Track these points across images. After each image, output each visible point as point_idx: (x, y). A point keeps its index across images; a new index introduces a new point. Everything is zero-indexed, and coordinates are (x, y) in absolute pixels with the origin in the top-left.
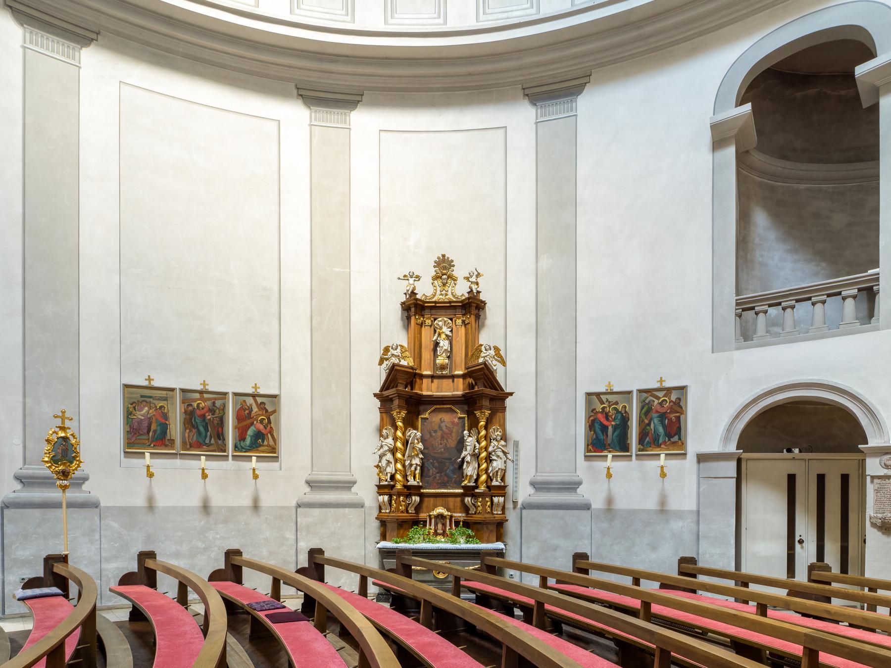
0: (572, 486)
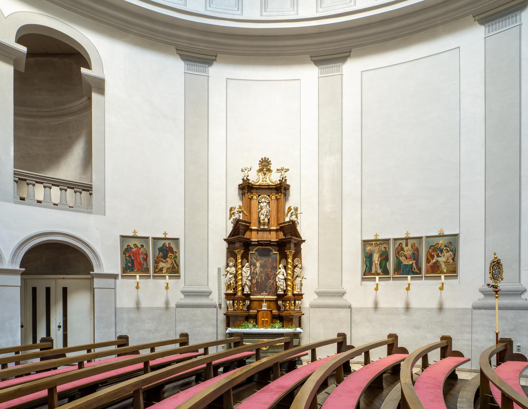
0: (342, 294)
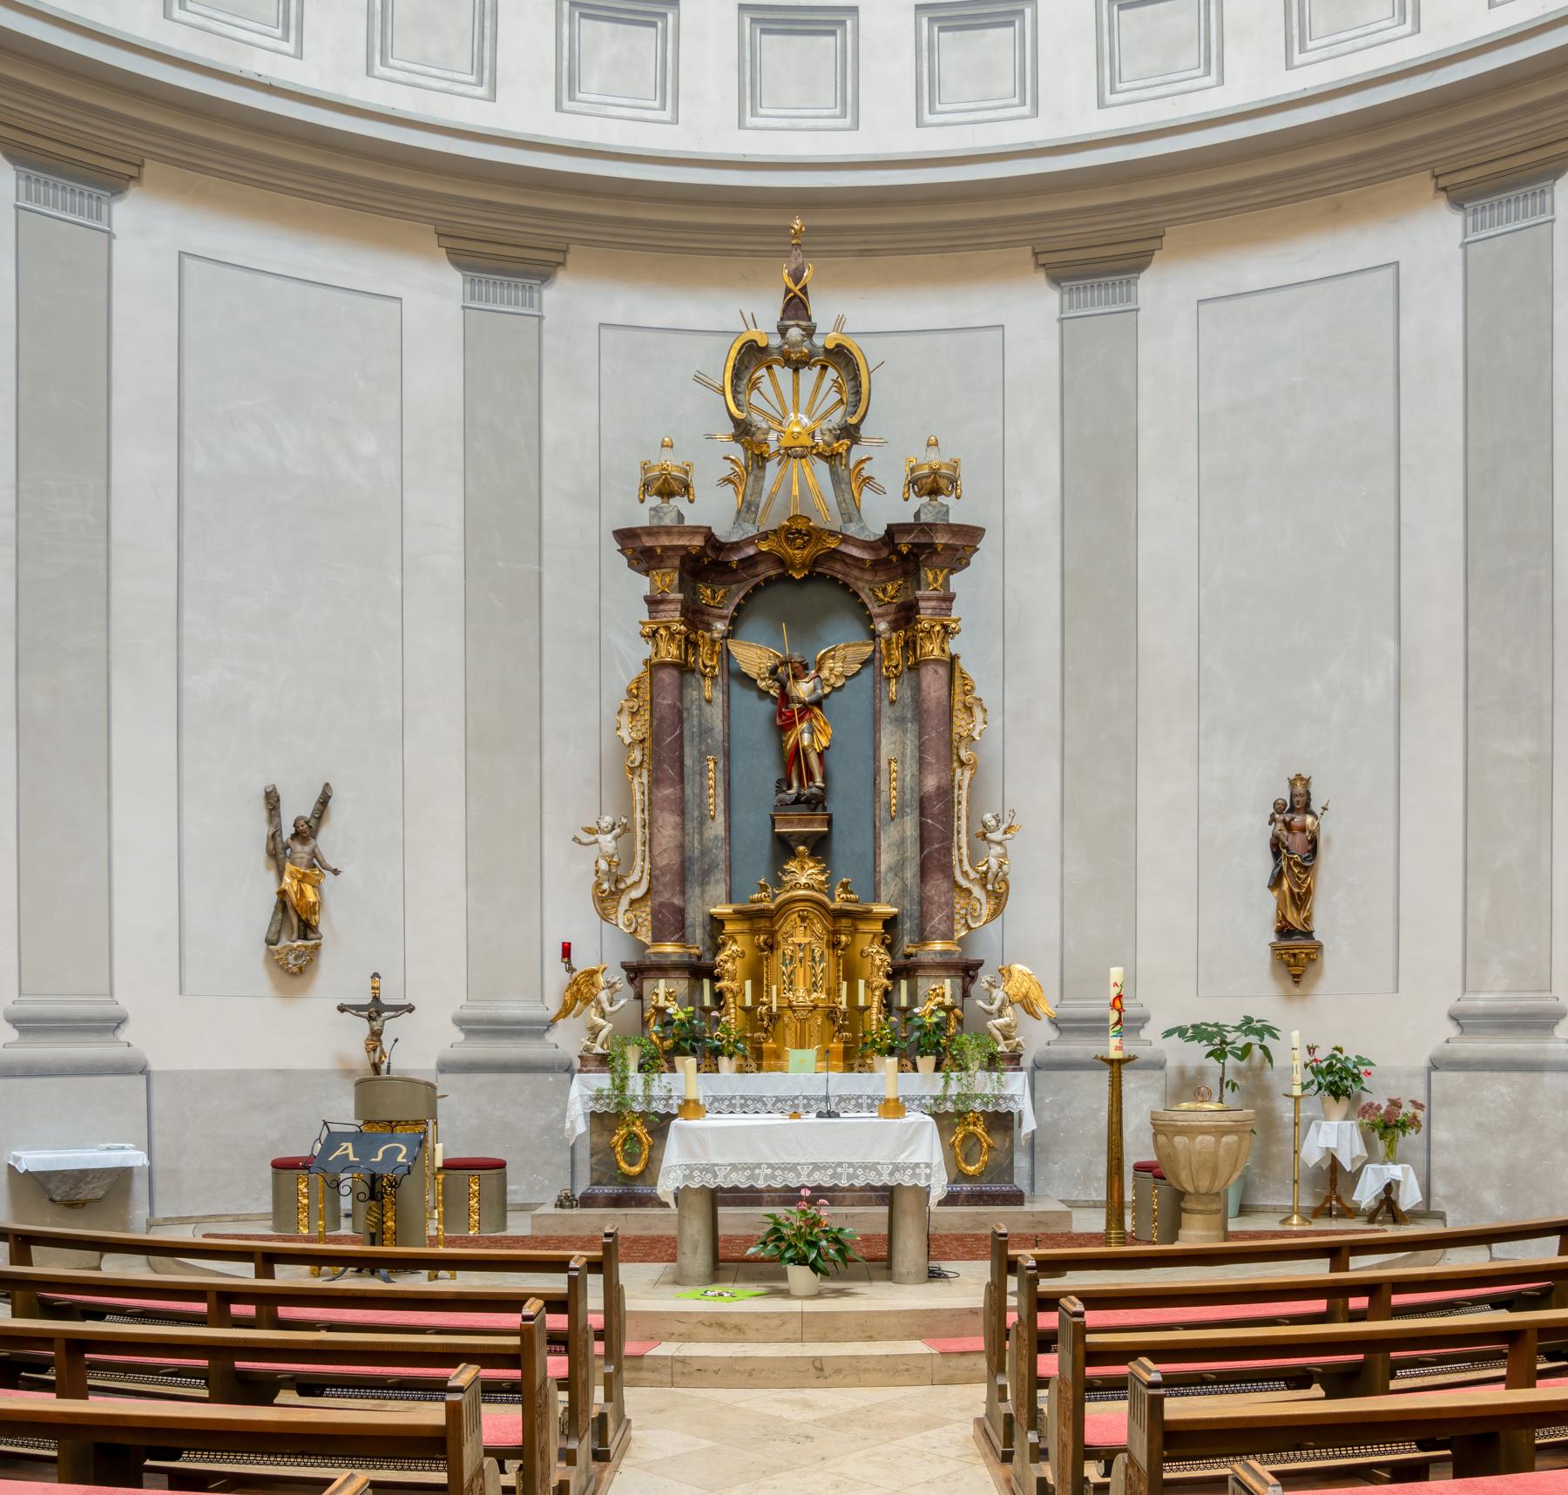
0: (112, 1025)
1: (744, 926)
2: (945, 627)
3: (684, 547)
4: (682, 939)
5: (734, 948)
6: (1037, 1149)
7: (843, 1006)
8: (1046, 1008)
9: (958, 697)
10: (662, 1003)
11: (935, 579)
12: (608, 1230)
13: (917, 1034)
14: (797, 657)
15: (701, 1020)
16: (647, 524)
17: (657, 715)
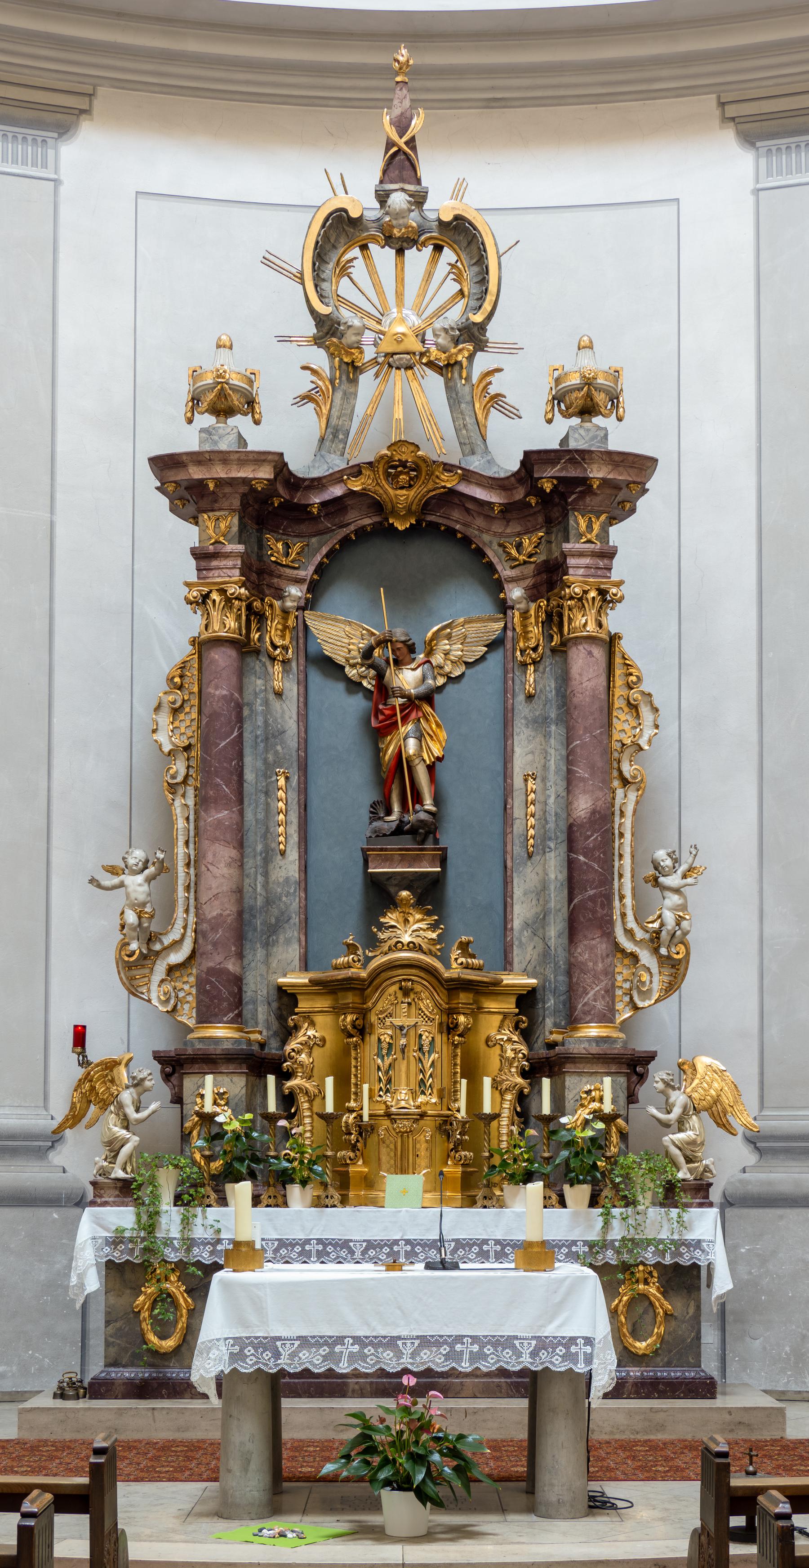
1: (322, 1003)
2: (602, 593)
3: (245, 481)
4: (239, 1020)
5: (310, 1033)
6: (729, 1318)
7: (462, 1115)
8: (744, 1117)
9: (619, 691)
10: (209, 1108)
11: (590, 527)
12: (99, 1444)
13: (565, 1153)
14: (399, 634)
15: (263, 1132)
16: (195, 448)
17: (206, 710)
